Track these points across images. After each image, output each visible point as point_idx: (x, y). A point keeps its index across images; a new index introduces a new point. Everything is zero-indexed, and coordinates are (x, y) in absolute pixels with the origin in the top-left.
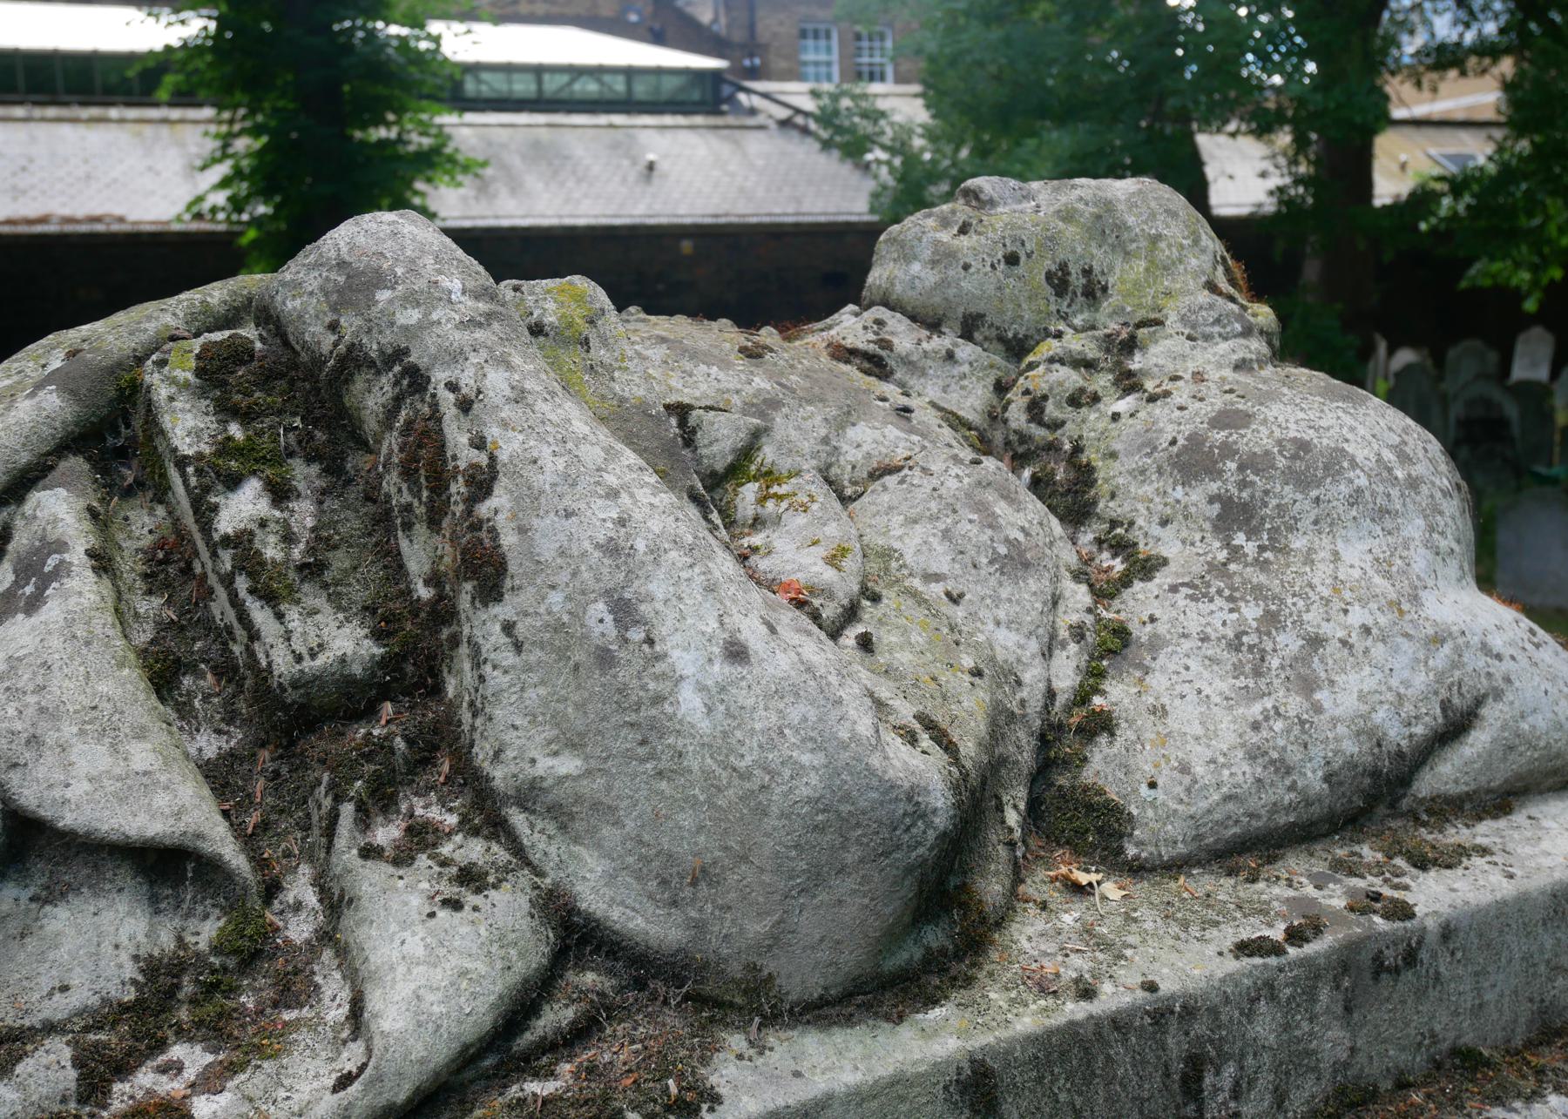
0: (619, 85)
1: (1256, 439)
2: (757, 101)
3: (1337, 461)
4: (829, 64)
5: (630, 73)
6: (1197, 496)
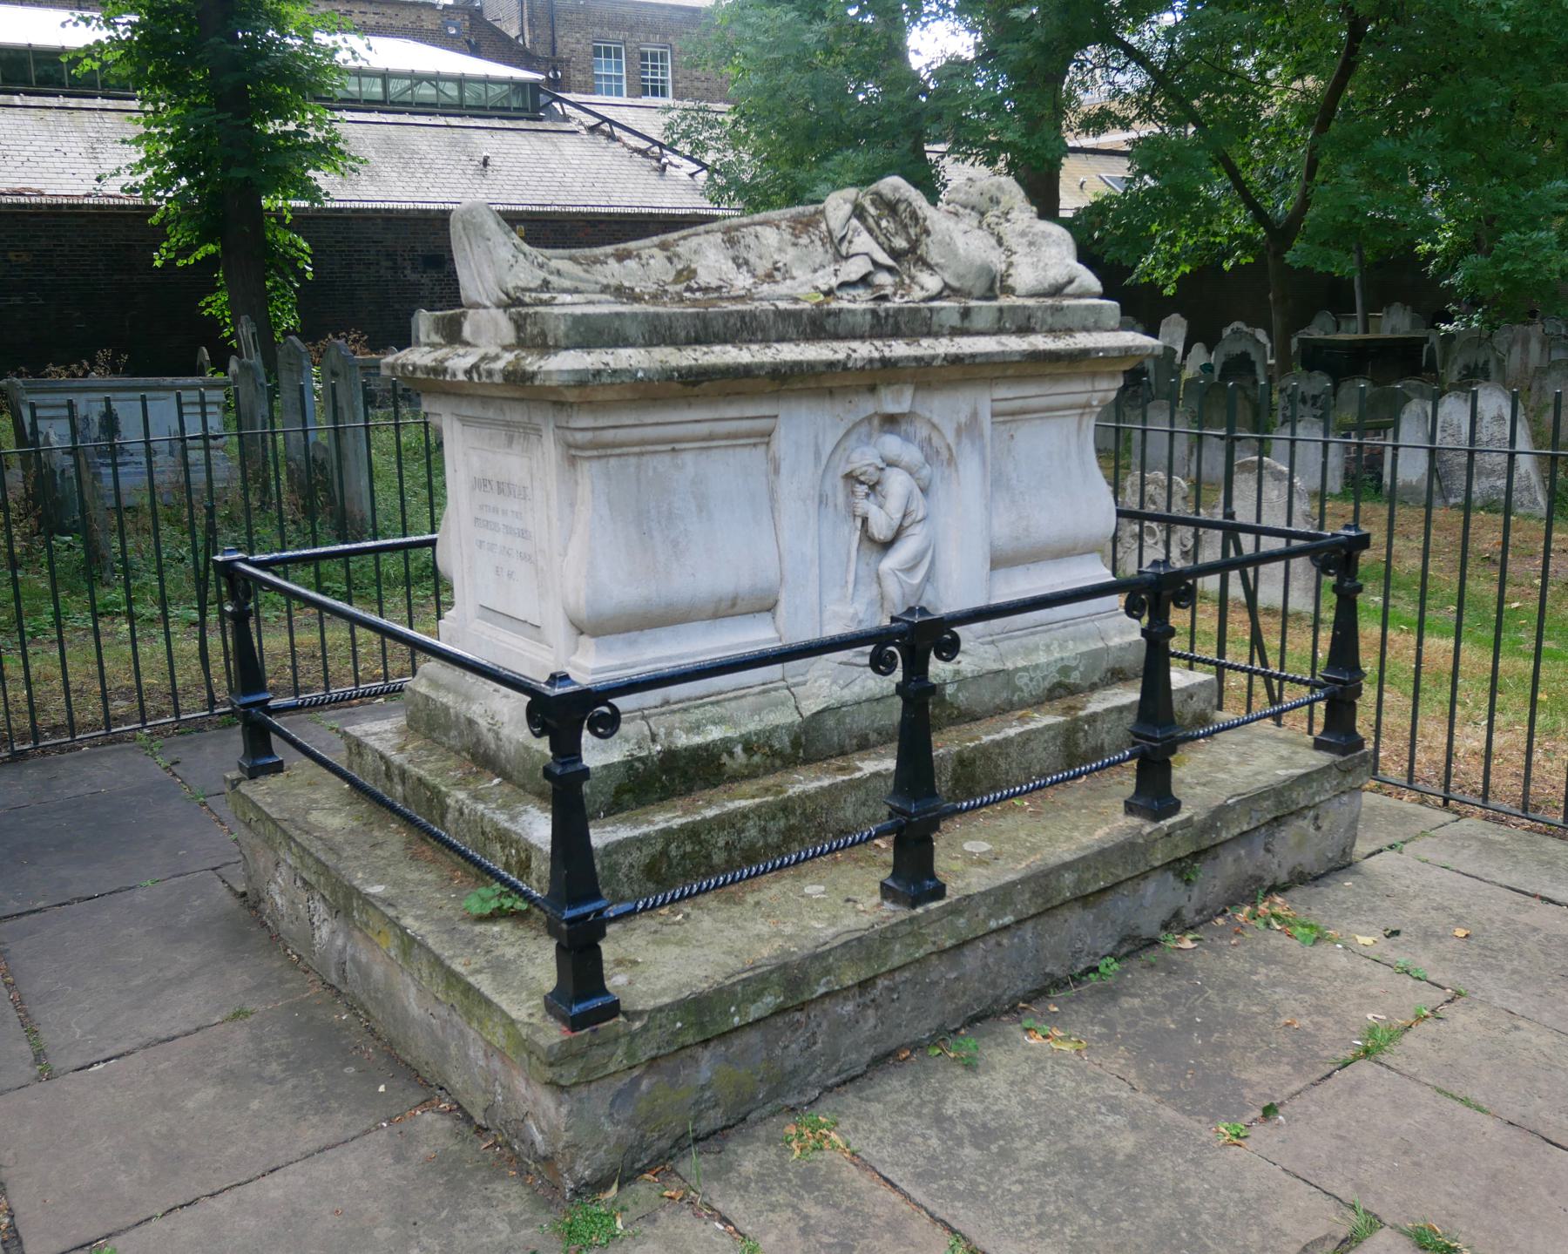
0: (452, 90)
1: (1034, 230)
2: (569, 110)
3: (1050, 235)
4: (619, 79)
5: (461, 81)
6: (1024, 240)
